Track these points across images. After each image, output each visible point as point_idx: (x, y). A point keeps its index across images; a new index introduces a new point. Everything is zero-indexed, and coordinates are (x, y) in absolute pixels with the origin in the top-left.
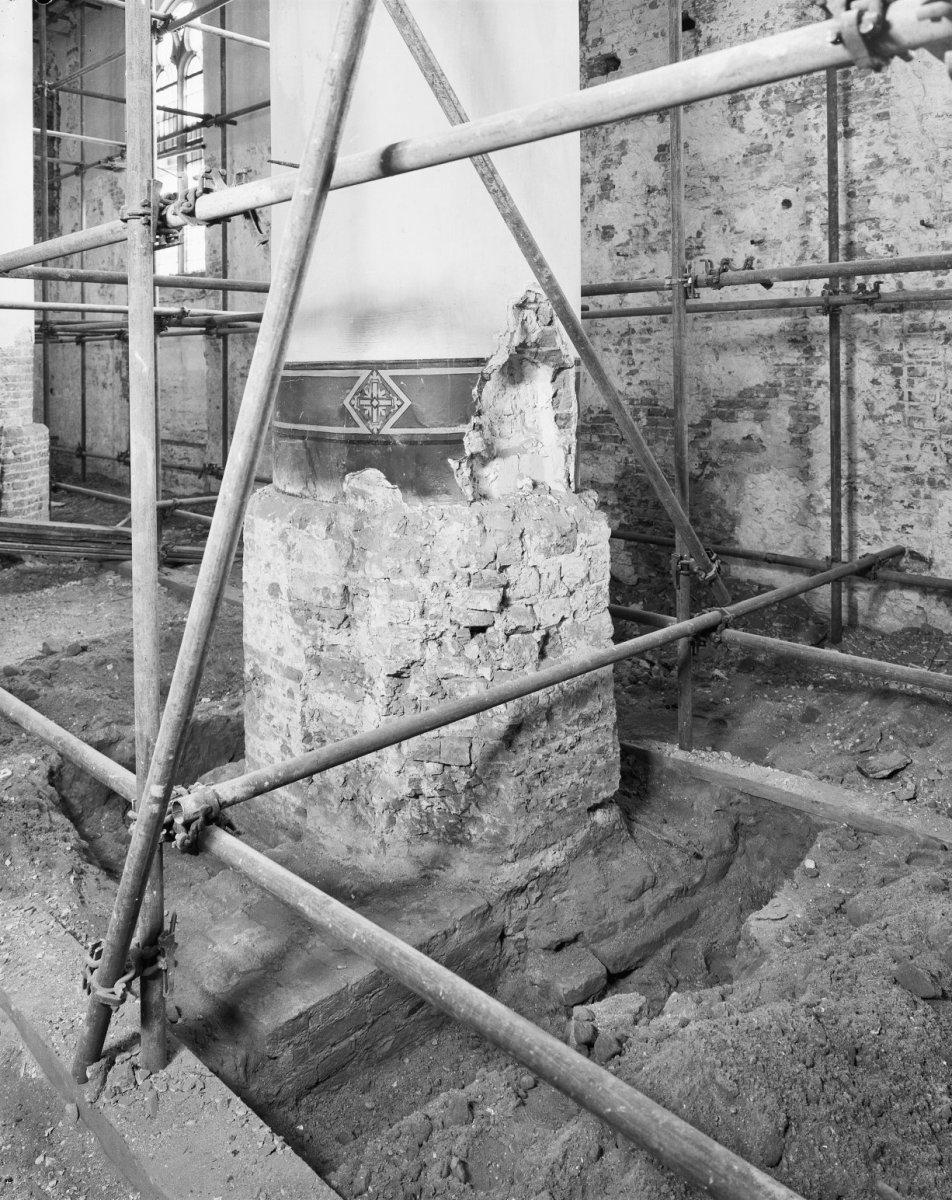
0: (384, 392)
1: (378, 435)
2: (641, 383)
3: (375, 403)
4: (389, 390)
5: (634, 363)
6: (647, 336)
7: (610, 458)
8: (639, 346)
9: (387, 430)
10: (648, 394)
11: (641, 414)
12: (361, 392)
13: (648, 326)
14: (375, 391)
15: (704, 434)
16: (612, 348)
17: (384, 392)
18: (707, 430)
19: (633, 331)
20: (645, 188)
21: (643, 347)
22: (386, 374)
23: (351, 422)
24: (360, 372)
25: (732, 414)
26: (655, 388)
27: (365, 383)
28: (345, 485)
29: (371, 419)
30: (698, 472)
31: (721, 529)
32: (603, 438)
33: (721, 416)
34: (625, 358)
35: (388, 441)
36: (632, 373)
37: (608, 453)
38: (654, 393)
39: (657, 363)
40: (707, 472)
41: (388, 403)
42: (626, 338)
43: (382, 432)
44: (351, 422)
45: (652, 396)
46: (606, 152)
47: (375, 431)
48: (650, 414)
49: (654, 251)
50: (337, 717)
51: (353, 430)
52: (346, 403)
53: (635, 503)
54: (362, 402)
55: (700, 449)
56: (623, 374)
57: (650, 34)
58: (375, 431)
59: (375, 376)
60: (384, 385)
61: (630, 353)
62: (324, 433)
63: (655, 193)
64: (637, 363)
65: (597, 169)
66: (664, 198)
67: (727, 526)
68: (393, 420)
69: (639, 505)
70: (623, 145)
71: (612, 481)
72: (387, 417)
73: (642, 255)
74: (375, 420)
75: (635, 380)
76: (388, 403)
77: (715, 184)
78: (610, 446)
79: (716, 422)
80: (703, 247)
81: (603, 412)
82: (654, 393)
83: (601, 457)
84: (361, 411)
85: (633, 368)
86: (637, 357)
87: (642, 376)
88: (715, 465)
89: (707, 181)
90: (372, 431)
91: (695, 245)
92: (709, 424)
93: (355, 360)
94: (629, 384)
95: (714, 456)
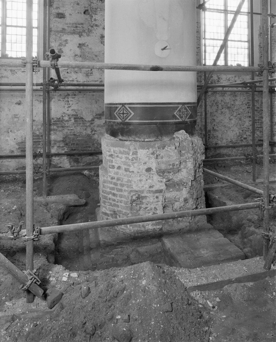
0: (185, 110)
1: (184, 121)
2: (72, 110)
3: (183, 113)
4: (187, 110)
5: (69, 104)
6: (74, 97)
7: (61, 132)
8: (71, 99)
9: (187, 120)
10: (74, 113)
11: (72, 119)
12: (180, 111)
13: (74, 94)
14: (184, 110)
15: (92, 123)
16: (61, 99)
17: (185, 110)
18: (93, 122)
19: (69, 95)
20: (74, 55)
21: (73, 100)
22: (186, 106)
23: (176, 118)
24: (179, 105)
25: (100, 117)
26: (77, 111)
27: (181, 108)
28: (174, 135)
29: (182, 117)
30: (91, 133)
31: (97, 147)
32: (58, 127)
33: (97, 118)
34: (67, 103)
35: (186, 122)
36: (69, 107)
37: (60, 131)
38: (76, 113)
39: (78, 104)
40: (93, 133)
41: (187, 113)
42: (67, 97)
43: (185, 120)
44: (176, 118)
45: (76, 114)
46: (60, 41)
47: (184, 120)
48: (75, 118)
49: (77, 73)
50: (172, 198)
51: (177, 121)
52: (175, 113)
53: (70, 145)
54: (180, 113)
55: (91, 127)
56: (66, 107)
57: (77, 12)
58: (184, 120)
59: (183, 106)
60: (186, 109)
61: (68, 101)
62: (167, 122)
63: (77, 57)
64: (71, 104)
65: (57, 46)
66: (80, 58)
67: (99, 147)
68: (188, 117)
69: (72, 145)
70: (66, 41)
71: (62, 139)
72: (186, 117)
73: (73, 73)
74: (183, 118)
75: (70, 109)
76: (187, 113)
77: (96, 57)
78: (60, 129)
79: (96, 120)
80: (92, 73)
81: (58, 119)
82: (76, 113)
83: (57, 133)
84: (180, 116)
85: (69, 105)
86: (71, 103)
87: (72, 108)
88: (95, 131)
89: (94, 56)
90: (183, 120)
91: (90, 72)
92: (94, 120)
93: (178, 102)
94: (68, 110)
95: (95, 129)
